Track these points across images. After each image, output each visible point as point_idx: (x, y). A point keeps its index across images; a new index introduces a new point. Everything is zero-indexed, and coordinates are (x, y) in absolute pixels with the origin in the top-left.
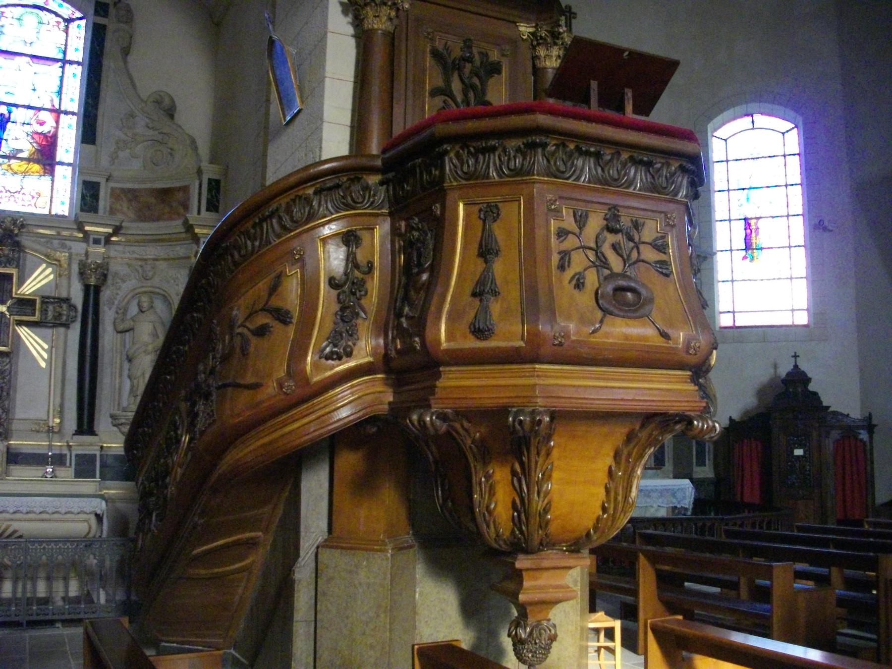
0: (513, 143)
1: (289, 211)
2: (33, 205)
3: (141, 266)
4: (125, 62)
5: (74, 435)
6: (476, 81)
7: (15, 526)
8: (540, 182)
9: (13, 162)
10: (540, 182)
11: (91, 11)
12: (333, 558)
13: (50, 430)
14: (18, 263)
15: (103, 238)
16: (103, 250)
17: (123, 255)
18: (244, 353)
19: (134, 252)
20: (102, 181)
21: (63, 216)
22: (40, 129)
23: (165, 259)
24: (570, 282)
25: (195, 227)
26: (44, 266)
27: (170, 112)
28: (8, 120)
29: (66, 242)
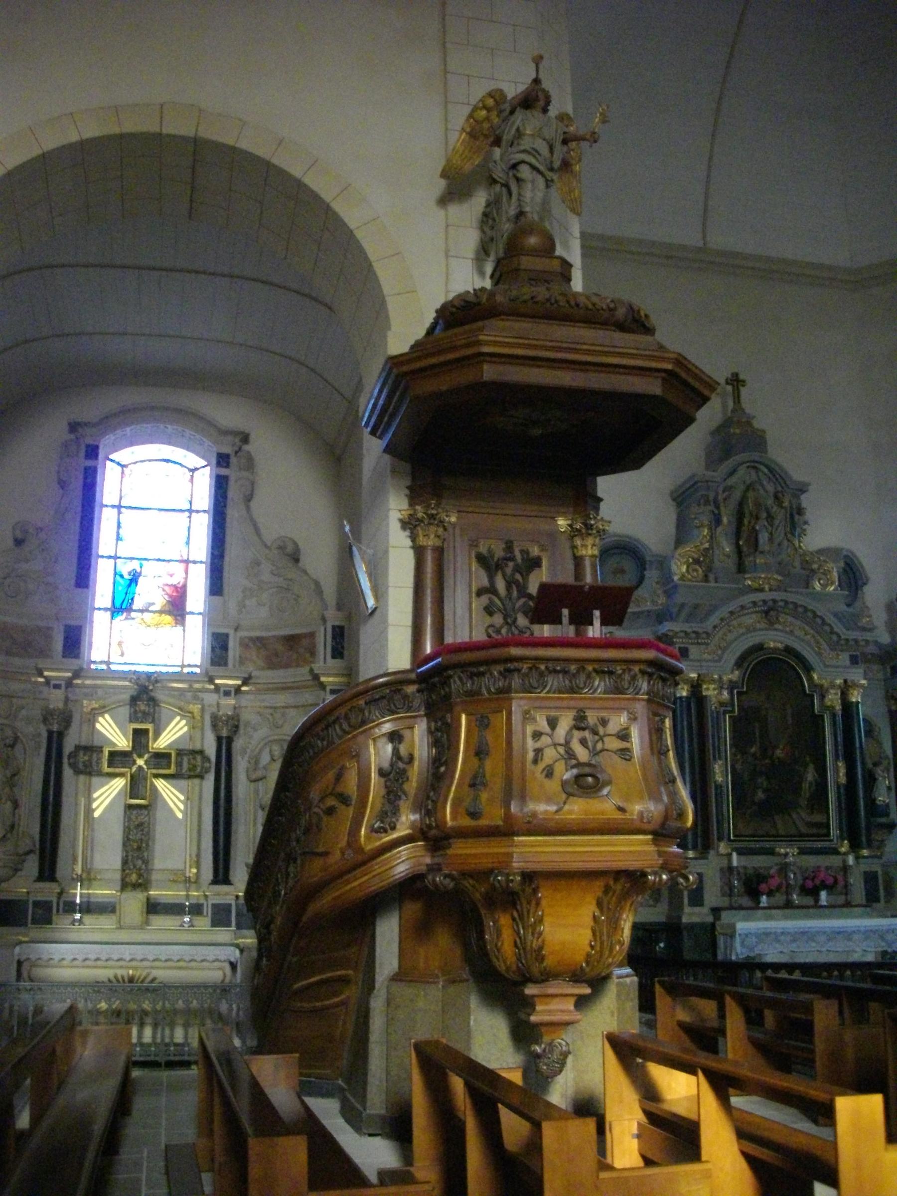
0: (496, 670)
1: (346, 717)
3: (272, 714)
4: (248, 508)
6: (518, 577)
7: (155, 973)
8: (517, 698)
10: (517, 698)
11: (214, 461)
12: (405, 991)
13: (188, 881)
15: (233, 690)
16: (233, 702)
18: (319, 829)
19: (264, 700)
20: (231, 632)
24: (542, 772)
26: (178, 718)
27: (295, 558)
28: (140, 574)
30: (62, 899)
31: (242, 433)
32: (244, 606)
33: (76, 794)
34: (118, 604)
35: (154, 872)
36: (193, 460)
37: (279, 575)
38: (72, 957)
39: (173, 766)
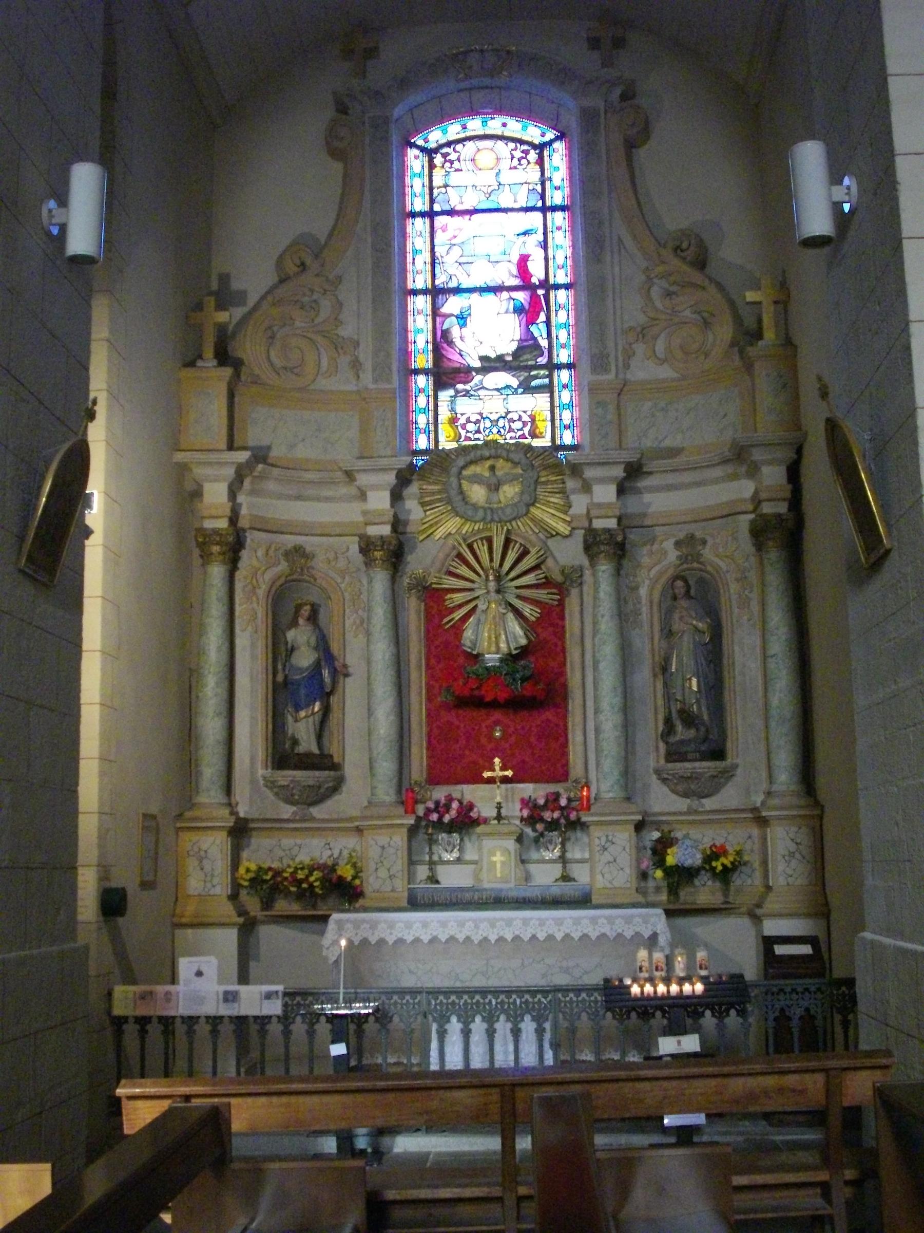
36: (534, 133)
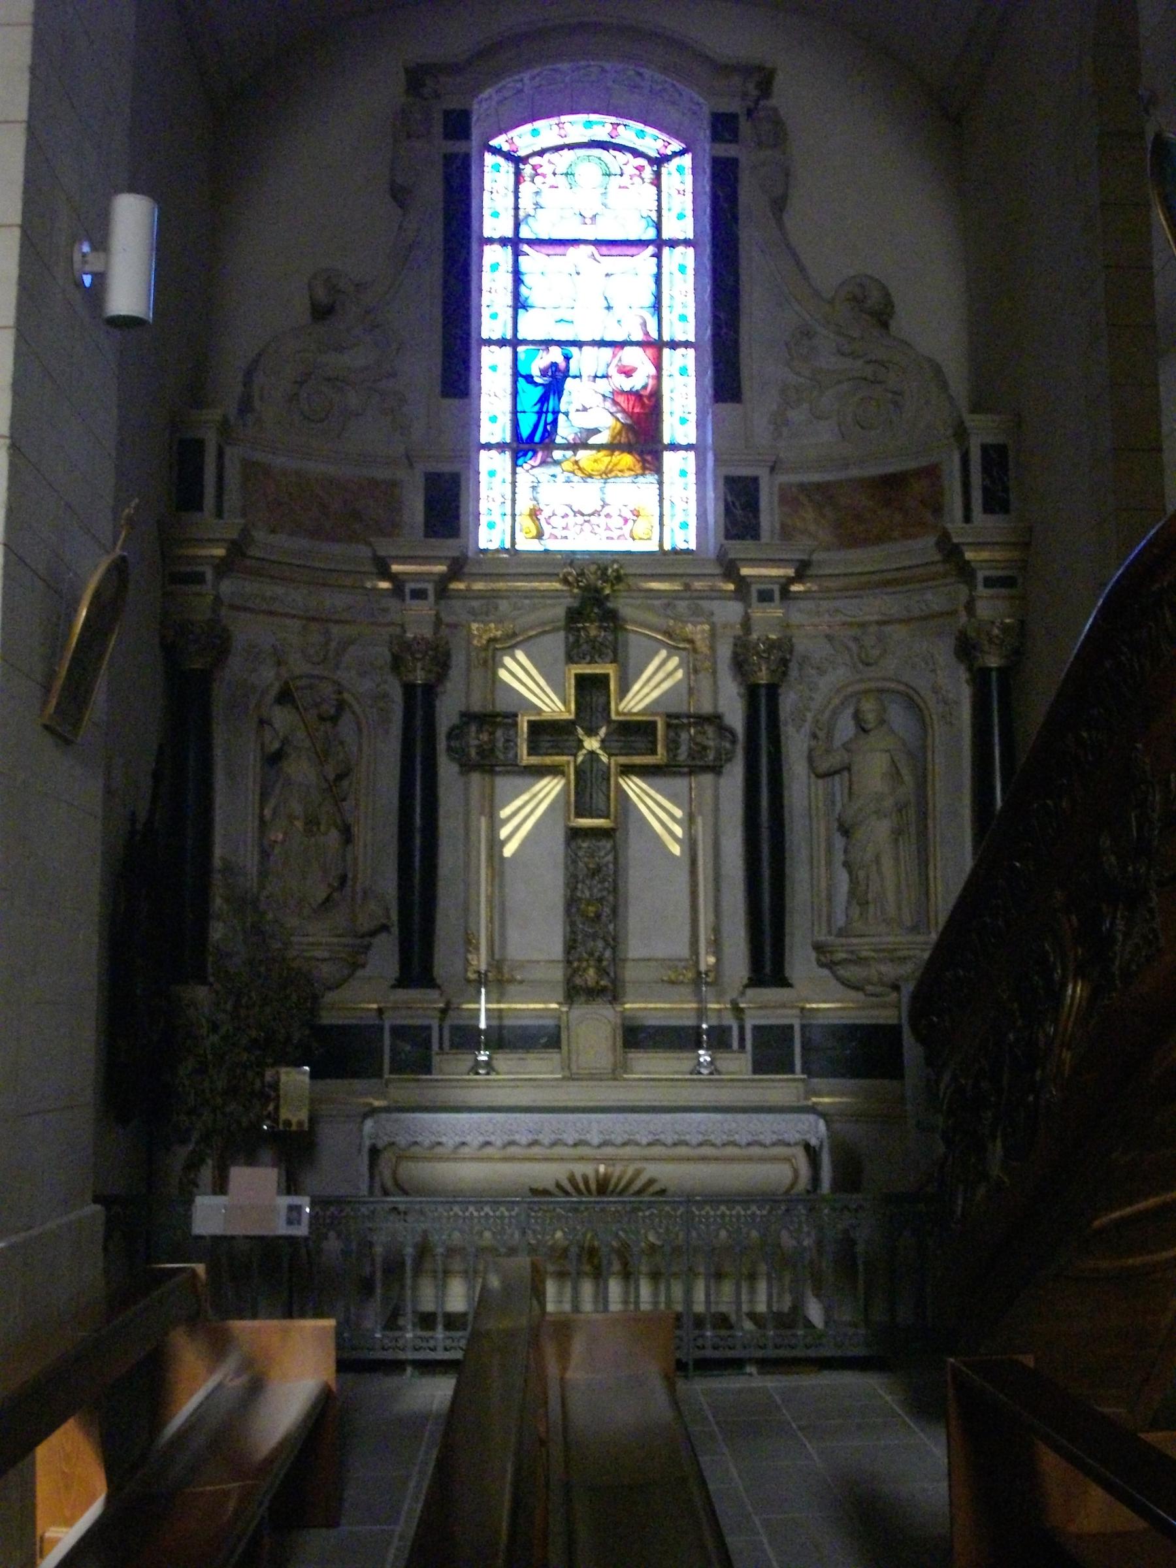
2: (627, 536)
3: (856, 639)
4: (779, 221)
5: (746, 986)
7: (652, 1170)
9: (583, 455)
11: (705, 134)
13: (698, 980)
14: (616, 654)
15: (776, 588)
16: (779, 613)
17: (816, 620)
19: (837, 611)
20: (763, 473)
21: (688, 552)
22: (627, 384)
23: (900, 621)
25: (964, 548)
26: (663, 653)
27: (883, 317)
28: (566, 374)
29: (701, 602)
30: (447, 1023)
31: (760, 68)
32: (786, 423)
33: (467, 813)
34: (525, 431)
35: (629, 965)
36: (652, 141)
37: (853, 355)
38: (481, 1139)
39: (660, 749)
